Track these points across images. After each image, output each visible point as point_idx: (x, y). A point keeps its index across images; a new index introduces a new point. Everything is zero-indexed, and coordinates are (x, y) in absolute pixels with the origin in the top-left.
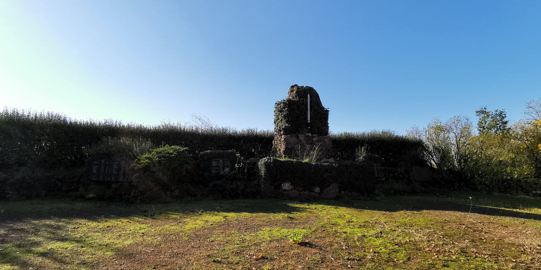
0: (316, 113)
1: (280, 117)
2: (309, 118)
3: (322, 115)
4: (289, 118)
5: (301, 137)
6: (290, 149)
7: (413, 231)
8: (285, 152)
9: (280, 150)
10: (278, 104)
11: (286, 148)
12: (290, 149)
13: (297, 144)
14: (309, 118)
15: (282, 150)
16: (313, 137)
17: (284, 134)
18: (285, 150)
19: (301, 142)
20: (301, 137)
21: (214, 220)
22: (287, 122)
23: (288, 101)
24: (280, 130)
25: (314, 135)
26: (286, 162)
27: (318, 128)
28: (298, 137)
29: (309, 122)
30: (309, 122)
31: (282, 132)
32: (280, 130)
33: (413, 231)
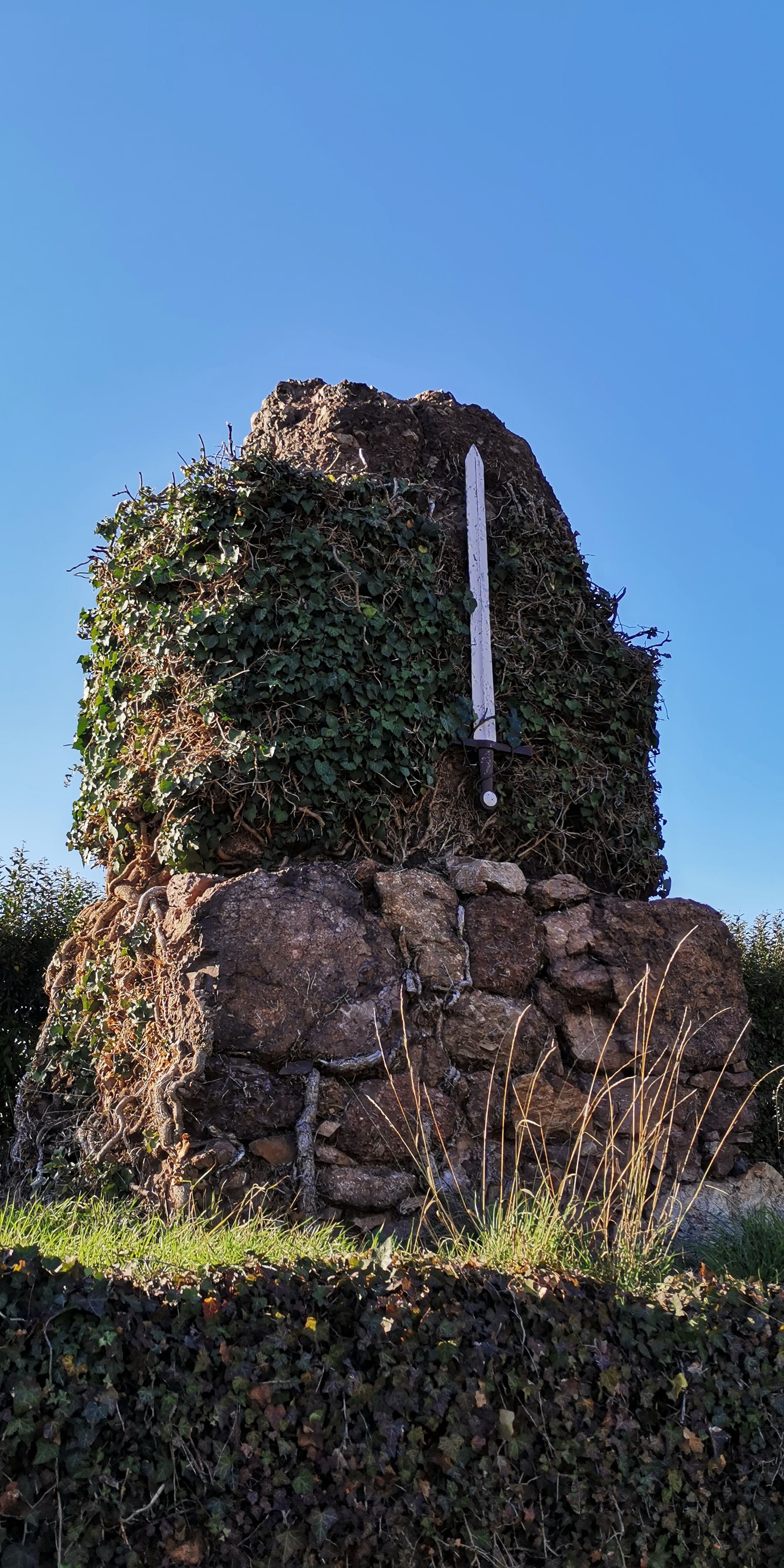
0: (560, 646)
1: (152, 660)
2: (483, 695)
3: (598, 692)
4: (244, 662)
5: (413, 898)
6: (271, 1063)
7: (96, 988)
8: (199, 1107)
9: (130, 1069)
10: (132, 524)
11: (227, 1043)
12: (271, 1063)
13: (368, 988)
14: (483, 695)
15: (165, 1072)
16: (541, 907)
17: (190, 862)
18: (210, 1073)
19: (408, 958)
20: (413, 898)
21: (196, 764)
22: (237, 710)
23: (248, 472)
24: (144, 820)
25: (553, 887)
26: (245, 1304)
27: (575, 818)
28: (372, 899)
29: (486, 733)
30: (486, 733)
31: (169, 842)
32: (144, 820)
33: (96, 988)
